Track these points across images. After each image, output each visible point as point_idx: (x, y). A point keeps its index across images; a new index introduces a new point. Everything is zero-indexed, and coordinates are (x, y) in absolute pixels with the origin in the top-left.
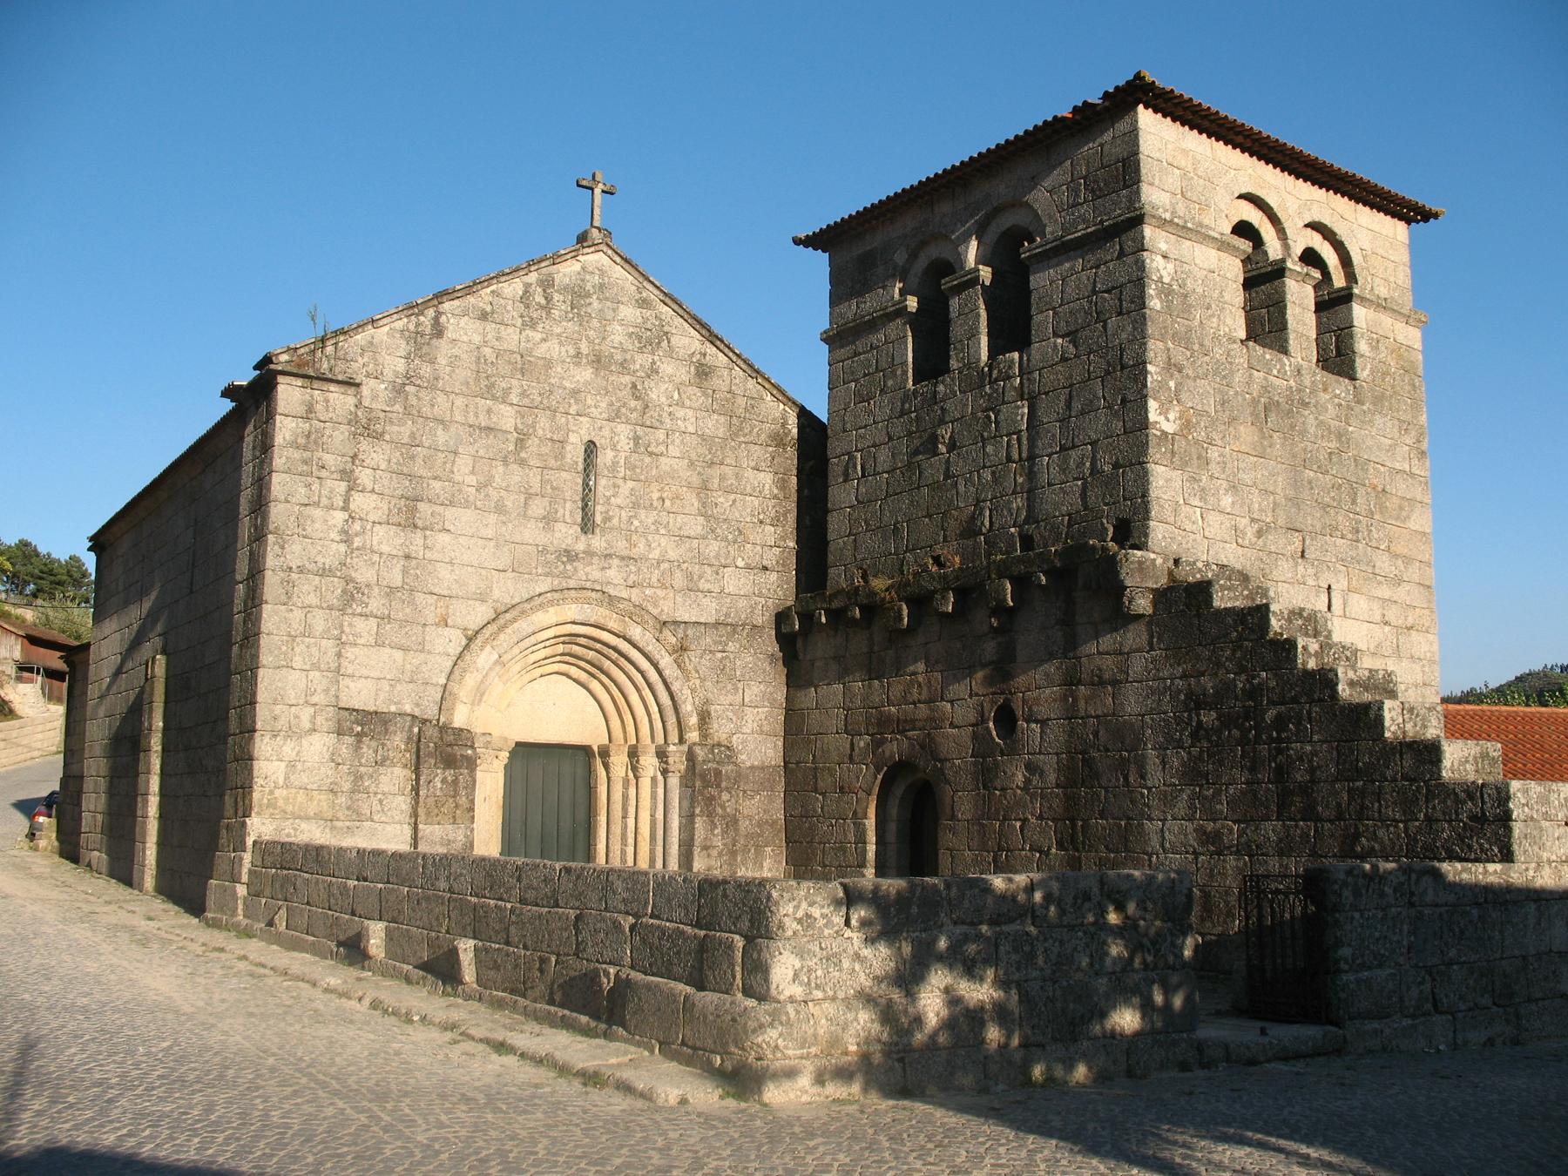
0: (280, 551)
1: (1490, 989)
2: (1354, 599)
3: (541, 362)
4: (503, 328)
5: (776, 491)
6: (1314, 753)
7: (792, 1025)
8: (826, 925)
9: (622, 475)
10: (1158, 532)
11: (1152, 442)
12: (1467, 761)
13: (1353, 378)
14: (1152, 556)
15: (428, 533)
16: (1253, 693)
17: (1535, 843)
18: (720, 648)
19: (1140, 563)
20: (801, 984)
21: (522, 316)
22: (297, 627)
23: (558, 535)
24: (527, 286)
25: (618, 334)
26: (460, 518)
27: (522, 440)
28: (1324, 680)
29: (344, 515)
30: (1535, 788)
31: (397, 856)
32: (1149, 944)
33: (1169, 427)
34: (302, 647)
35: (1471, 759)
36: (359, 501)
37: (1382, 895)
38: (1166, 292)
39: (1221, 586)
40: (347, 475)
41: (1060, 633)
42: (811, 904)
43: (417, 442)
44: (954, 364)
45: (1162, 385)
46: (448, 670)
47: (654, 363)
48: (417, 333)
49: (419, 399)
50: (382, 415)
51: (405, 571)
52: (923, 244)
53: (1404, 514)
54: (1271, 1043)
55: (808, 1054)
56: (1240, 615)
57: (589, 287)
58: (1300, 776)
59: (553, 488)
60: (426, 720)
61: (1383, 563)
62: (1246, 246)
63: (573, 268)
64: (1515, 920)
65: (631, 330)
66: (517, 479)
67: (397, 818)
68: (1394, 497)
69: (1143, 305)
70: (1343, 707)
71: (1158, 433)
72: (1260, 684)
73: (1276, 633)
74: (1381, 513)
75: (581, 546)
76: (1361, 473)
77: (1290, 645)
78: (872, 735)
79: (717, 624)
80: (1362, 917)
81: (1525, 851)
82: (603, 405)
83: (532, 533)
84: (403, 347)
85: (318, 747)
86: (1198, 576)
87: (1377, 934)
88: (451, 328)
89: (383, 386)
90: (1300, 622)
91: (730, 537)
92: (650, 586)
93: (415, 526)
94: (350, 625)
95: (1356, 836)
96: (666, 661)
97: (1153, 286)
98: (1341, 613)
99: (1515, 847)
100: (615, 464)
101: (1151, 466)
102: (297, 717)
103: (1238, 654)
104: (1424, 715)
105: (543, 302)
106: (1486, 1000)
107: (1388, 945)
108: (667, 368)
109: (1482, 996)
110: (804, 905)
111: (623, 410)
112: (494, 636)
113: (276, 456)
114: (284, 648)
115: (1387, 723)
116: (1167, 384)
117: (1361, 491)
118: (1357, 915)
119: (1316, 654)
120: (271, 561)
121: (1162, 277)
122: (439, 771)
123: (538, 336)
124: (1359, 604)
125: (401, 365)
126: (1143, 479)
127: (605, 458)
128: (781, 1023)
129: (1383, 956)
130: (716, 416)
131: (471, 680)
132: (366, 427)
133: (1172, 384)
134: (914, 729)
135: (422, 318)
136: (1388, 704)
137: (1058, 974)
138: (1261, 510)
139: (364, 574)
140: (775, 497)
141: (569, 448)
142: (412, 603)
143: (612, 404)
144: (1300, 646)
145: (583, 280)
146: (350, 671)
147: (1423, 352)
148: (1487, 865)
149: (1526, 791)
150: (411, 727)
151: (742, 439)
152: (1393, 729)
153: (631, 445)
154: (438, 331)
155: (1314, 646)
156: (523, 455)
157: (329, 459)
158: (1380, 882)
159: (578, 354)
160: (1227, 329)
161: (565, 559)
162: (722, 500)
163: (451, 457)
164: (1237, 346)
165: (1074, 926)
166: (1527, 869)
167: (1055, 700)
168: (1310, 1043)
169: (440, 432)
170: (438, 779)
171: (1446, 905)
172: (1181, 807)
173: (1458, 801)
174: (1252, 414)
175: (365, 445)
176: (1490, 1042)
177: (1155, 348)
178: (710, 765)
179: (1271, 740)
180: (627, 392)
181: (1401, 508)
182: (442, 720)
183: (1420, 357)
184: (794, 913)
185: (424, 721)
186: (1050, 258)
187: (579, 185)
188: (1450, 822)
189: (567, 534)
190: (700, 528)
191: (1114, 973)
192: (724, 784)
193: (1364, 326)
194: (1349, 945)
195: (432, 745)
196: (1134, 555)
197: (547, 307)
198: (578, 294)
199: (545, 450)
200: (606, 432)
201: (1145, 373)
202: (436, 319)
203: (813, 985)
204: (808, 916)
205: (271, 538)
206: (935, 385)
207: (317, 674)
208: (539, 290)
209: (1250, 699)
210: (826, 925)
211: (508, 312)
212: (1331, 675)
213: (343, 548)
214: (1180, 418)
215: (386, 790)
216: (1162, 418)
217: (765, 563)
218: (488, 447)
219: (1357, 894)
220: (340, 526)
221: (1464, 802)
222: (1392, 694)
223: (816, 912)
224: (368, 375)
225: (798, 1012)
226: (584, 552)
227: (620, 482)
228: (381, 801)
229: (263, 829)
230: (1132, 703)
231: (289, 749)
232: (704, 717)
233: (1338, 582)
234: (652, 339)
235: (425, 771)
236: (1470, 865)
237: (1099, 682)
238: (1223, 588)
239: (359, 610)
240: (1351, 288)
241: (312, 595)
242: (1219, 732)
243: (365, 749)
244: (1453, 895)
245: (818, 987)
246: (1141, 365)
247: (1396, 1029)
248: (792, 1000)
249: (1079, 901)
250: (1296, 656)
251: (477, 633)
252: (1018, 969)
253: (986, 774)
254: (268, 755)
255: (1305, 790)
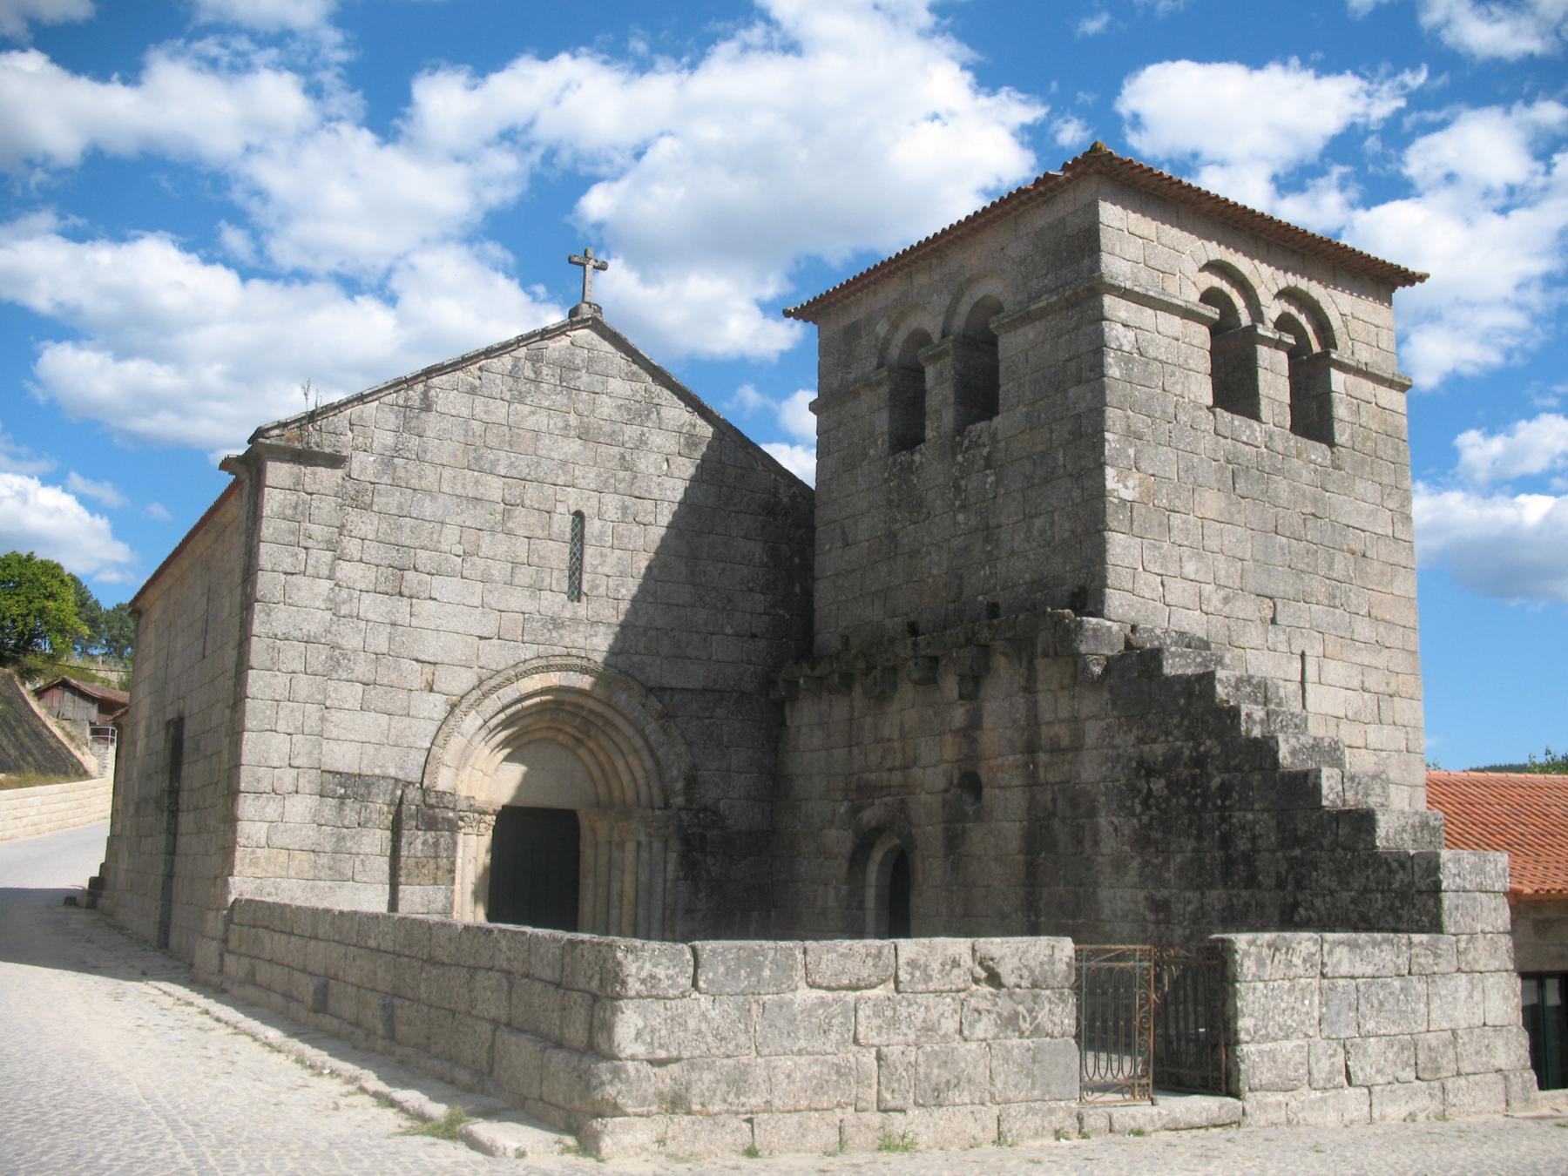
0: (266, 618)
1: (1413, 1062)
2: (1330, 665)
3: (529, 435)
4: (491, 401)
5: (765, 560)
6: (1255, 822)
7: (631, 1084)
8: (671, 986)
9: (610, 544)
10: (1115, 601)
11: (1110, 510)
12: (1404, 830)
13: (1331, 444)
14: (1108, 623)
15: (414, 600)
16: (1199, 761)
17: (1468, 914)
18: (708, 714)
19: (1095, 630)
20: (644, 1042)
21: (510, 390)
22: (282, 692)
23: (544, 603)
24: (517, 359)
25: (606, 407)
26: (444, 587)
27: (509, 511)
28: (1265, 748)
29: (329, 584)
30: (1469, 857)
31: (375, 917)
32: (1025, 1012)
33: (1127, 495)
34: (287, 711)
35: (1408, 828)
36: (345, 570)
37: (1290, 965)
38: (1127, 360)
39: (1172, 653)
40: (331, 545)
41: (1022, 701)
42: (656, 965)
43: (405, 513)
44: (929, 433)
45: (1120, 452)
46: (432, 735)
47: (643, 434)
48: (407, 407)
49: (407, 471)
50: (370, 487)
51: (391, 639)
52: (903, 315)
53: (1385, 580)
54: (1159, 1113)
55: (649, 1112)
56: (1186, 682)
57: (578, 361)
58: (1243, 845)
59: (540, 557)
60: (410, 783)
61: (1364, 629)
62: (1213, 313)
63: (563, 343)
64: (1443, 992)
65: (620, 402)
66: (505, 548)
67: (378, 879)
68: (1375, 563)
69: (1103, 375)
70: (1283, 775)
71: (1116, 501)
72: (1205, 752)
73: (1221, 700)
74: (1361, 578)
75: (567, 614)
76: (1338, 538)
77: (1234, 713)
78: (852, 801)
79: (704, 690)
80: (1266, 987)
81: (1456, 923)
82: (592, 476)
83: (517, 600)
84: (392, 421)
85: (301, 808)
86: (1156, 643)
87: (1283, 1005)
88: (439, 402)
89: (372, 459)
90: (1248, 689)
91: (719, 605)
92: (637, 653)
93: (401, 594)
94: (336, 690)
95: (1295, 905)
96: (652, 727)
97: (1112, 355)
98: (1316, 679)
99: (1445, 918)
100: (602, 533)
101: (1108, 534)
102: (280, 779)
103: (1186, 722)
104: (1366, 784)
105: (532, 376)
106: (1409, 1074)
107: (1295, 1017)
108: (656, 439)
109: (1403, 1069)
110: (648, 966)
111: (612, 481)
112: (479, 702)
113: (264, 527)
114: (268, 712)
115: (1325, 791)
116: (1126, 451)
117: (1339, 557)
118: (1260, 985)
119: (1262, 722)
120: (257, 628)
121: (1121, 345)
122: (420, 833)
123: (527, 409)
124: (1336, 671)
125: (389, 439)
126: (1100, 548)
127: (593, 527)
128: (620, 1081)
129: (1290, 1027)
130: (705, 486)
131: (456, 743)
132: (357, 499)
133: (1131, 452)
134: (888, 795)
135: (411, 393)
136: (1326, 772)
137: (923, 1039)
138: (1228, 576)
139: (351, 641)
140: (766, 565)
141: (556, 517)
142: (398, 668)
143: (599, 475)
144: (1243, 716)
145: (572, 354)
146: (334, 735)
147: (1409, 416)
148: (1412, 936)
149: (1458, 861)
150: (394, 790)
151: (731, 508)
152: (1331, 797)
153: (619, 515)
154: (427, 406)
155: (1259, 713)
156: (510, 525)
157: (317, 531)
158: (1287, 953)
159: (567, 426)
160: (1192, 397)
161: (551, 627)
162: (710, 568)
163: (438, 527)
164: (1204, 413)
165: (942, 992)
166: (1458, 941)
167: (1017, 767)
168: (1204, 1115)
169: (427, 503)
170: (416, 842)
171: (1363, 977)
172: (1132, 876)
173: (1390, 871)
174: (1218, 481)
175: (353, 515)
176: (1412, 1117)
177: (1112, 414)
178: (695, 829)
179: (1217, 808)
180: (615, 463)
181: (1383, 573)
182: (426, 783)
183: (1405, 421)
184: (638, 973)
185: (408, 784)
186: (1016, 327)
187: (570, 261)
188: (1383, 892)
189: (554, 602)
190: (688, 595)
191: (985, 1040)
192: (709, 849)
193: (1343, 391)
194: (1251, 1015)
195: (413, 807)
196: (1088, 622)
197: (536, 382)
198: (566, 368)
199: (532, 520)
200: (594, 502)
201: (1103, 440)
202: (425, 394)
203: (656, 1044)
204: (652, 977)
205: (258, 606)
206: (912, 454)
207: (300, 736)
208: (529, 364)
209: (1196, 766)
210: (671, 986)
211: (497, 386)
212: (1272, 743)
213: (328, 615)
214: (1140, 486)
215: (368, 850)
216: (1121, 485)
217: (754, 630)
218: (474, 517)
219: (1260, 963)
220: (326, 593)
221: (1395, 872)
222: (1338, 763)
223: (661, 972)
224: (356, 449)
225: (638, 1071)
226: (571, 619)
227: (607, 551)
228: (363, 862)
229: (245, 887)
230: (1090, 771)
231: (271, 809)
232: (691, 782)
233: (1312, 648)
234: (642, 412)
235: (406, 835)
236: (1392, 935)
237: (1056, 750)
238: (1173, 655)
239: (344, 676)
240: (1329, 353)
241: (297, 660)
242: (1168, 800)
243: (347, 811)
244: (1371, 966)
245: (661, 1046)
246: (1099, 430)
247: (1303, 1102)
248: (633, 1058)
249: (948, 968)
250: (1239, 723)
251: (462, 697)
252: (879, 1034)
253: (953, 842)
254: (250, 815)
255: (1248, 858)
